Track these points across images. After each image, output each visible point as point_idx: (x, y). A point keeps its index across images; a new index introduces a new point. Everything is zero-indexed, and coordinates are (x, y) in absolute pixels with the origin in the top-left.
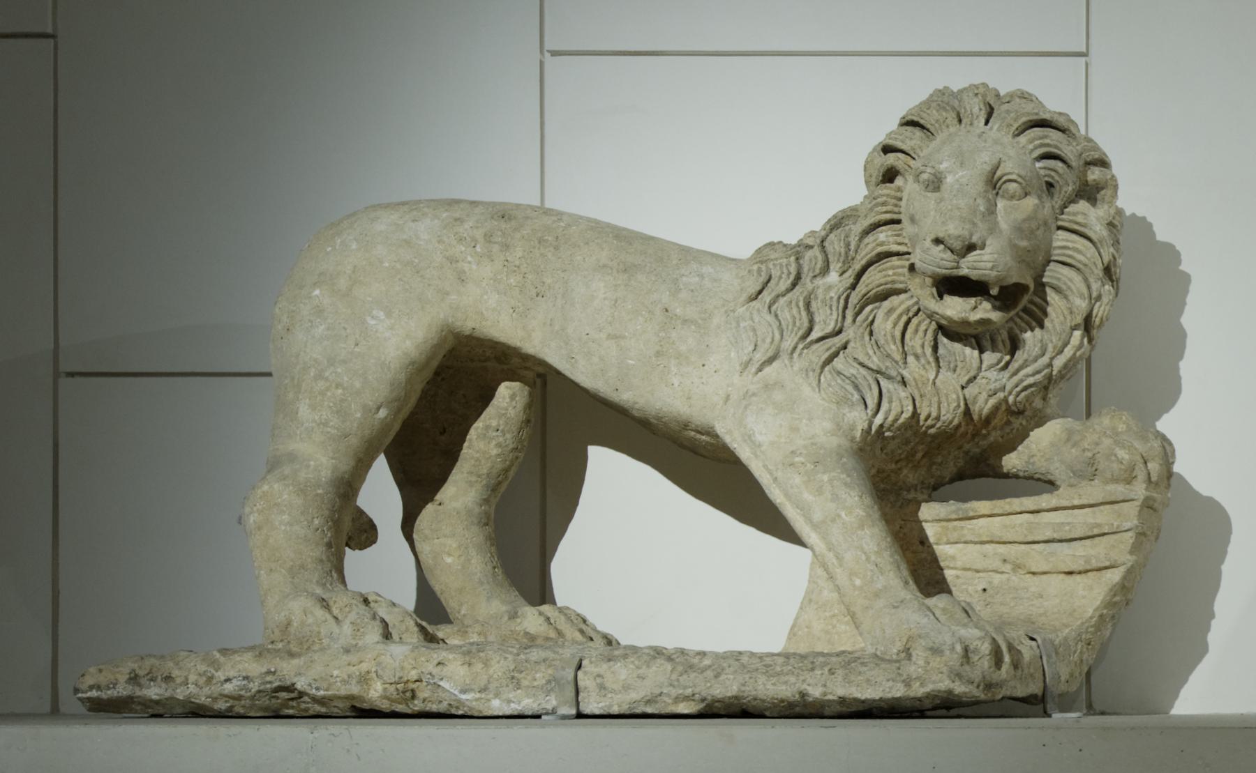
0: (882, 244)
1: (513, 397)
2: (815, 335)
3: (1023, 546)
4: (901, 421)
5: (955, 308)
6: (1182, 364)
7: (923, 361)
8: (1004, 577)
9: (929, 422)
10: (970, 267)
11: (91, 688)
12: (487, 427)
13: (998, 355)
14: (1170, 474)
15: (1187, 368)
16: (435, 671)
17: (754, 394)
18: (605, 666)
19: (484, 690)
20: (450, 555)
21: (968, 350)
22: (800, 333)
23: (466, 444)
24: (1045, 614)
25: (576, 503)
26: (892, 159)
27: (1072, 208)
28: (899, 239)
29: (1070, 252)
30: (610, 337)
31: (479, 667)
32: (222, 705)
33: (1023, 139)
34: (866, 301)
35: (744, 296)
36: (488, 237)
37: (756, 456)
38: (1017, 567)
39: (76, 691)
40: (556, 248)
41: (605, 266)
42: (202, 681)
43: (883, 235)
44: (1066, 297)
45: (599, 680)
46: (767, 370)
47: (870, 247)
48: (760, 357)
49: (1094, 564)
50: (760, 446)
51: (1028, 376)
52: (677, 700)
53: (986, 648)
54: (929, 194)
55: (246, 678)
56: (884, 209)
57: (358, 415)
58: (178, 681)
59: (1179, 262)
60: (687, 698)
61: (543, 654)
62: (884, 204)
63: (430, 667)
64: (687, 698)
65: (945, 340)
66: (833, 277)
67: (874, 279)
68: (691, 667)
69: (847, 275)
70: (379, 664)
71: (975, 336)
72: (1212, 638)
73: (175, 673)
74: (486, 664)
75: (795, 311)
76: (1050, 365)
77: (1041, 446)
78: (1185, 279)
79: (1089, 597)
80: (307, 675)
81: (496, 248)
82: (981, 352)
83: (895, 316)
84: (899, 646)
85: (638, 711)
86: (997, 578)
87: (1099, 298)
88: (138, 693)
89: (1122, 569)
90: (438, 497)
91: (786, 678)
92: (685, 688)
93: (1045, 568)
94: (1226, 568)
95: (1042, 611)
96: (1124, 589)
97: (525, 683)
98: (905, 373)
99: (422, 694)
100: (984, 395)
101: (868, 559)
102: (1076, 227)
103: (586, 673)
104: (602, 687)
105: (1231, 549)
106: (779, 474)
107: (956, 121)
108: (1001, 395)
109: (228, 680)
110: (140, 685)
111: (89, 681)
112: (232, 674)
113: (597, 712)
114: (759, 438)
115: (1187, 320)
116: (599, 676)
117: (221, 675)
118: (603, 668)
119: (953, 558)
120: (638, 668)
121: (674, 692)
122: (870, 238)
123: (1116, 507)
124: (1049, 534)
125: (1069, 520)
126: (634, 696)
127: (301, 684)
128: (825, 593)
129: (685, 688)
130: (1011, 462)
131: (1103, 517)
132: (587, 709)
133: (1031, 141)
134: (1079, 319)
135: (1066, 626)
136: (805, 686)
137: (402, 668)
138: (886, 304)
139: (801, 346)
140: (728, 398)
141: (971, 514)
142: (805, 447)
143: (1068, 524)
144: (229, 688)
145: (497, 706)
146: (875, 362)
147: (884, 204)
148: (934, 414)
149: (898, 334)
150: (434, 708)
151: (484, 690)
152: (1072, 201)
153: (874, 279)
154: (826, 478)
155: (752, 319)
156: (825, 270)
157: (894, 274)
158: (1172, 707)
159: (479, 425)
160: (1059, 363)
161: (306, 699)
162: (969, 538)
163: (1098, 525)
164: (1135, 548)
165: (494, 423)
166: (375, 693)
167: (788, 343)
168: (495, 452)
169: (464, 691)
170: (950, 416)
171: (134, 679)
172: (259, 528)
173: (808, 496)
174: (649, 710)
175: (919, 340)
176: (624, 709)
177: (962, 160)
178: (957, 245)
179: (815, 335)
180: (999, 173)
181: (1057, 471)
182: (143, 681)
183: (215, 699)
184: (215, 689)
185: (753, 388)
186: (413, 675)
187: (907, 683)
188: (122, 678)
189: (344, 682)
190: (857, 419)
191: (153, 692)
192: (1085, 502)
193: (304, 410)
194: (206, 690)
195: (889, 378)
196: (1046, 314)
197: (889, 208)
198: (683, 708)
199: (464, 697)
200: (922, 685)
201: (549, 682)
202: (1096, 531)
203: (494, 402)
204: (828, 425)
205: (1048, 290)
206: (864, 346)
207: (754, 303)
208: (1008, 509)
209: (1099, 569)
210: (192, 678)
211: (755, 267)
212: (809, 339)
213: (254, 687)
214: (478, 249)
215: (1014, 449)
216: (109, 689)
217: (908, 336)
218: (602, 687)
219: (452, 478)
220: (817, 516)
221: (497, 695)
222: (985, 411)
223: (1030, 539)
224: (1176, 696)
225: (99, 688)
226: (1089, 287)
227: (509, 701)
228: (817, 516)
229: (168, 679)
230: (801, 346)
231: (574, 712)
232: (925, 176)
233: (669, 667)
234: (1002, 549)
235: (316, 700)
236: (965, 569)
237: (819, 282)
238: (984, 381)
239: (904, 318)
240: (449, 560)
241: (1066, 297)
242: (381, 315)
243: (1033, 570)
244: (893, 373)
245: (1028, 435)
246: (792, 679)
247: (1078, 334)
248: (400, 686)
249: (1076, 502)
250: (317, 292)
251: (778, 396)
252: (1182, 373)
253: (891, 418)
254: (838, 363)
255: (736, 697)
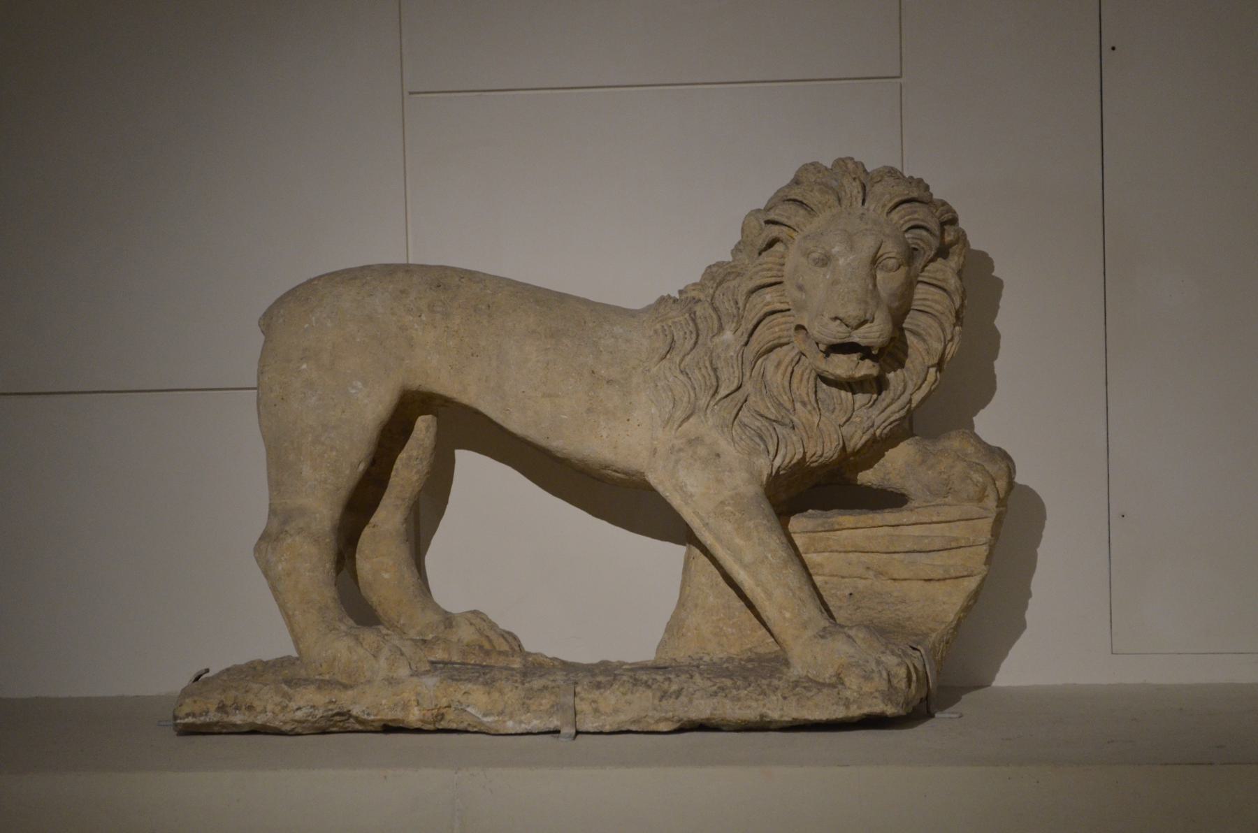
0: (768, 304)
1: (427, 428)
2: (723, 392)
3: (885, 556)
4: (795, 461)
5: (842, 366)
6: (996, 363)
7: (809, 407)
8: (869, 582)
9: (814, 458)
10: (857, 337)
11: (188, 715)
12: (410, 458)
13: (867, 396)
14: (1011, 484)
15: (1001, 366)
16: (463, 699)
17: (680, 450)
18: (597, 693)
19: (501, 713)
20: (387, 571)
21: (843, 393)
22: (711, 392)
23: (393, 473)
24: (909, 619)
25: (446, 503)
26: (775, 231)
27: (931, 266)
28: (783, 299)
29: (928, 303)
30: (544, 395)
31: (496, 695)
32: (288, 728)
33: (895, 216)
34: (760, 355)
35: (657, 358)
36: (431, 307)
37: (687, 504)
38: (879, 574)
39: (175, 718)
40: (490, 316)
41: (534, 332)
42: (277, 709)
43: (769, 296)
44: (924, 341)
45: (594, 705)
46: (686, 425)
47: (759, 306)
48: (679, 414)
49: (953, 573)
50: (691, 496)
51: (894, 413)
52: (658, 721)
53: (902, 672)
54: (818, 269)
55: (313, 707)
56: (770, 274)
57: (347, 472)
58: (259, 709)
59: (992, 268)
60: (667, 719)
61: (543, 682)
62: (769, 270)
63: (459, 696)
64: (667, 719)
65: (824, 386)
66: (728, 335)
67: (764, 336)
68: (665, 692)
69: (739, 333)
70: (418, 694)
71: (852, 385)
72: (1029, 616)
73: (256, 703)
74: (501, 692)
75: (704, 371)
76: (910, 401)
77: (895, 467)
78: (998, 284)
79: (948, 602)
80: (361, 704)
81: (438, 316)
82: (854, 393)
83: (782, 368)
84: (831, 671)
85: (624, 729)
86: (861, 584)
87: (952, 340)
88: (226, 719)
89: (978, 579)
90: (372, 520)
91: (749, 703)
92: (666, 712)
93: (907, 576)
94: (1041, 551)
95: (907, 615)
96: (976, 595)
97: (533, 707)
98: (795, 419)
99: (448, 717)
100: (860, 432)
101: (794, 594)
102: (934, 282)
103: (582, 699)
104: (596, 710)
105: (1046, 533)
106: (711, 521)
107: (836, 203)
108: (872, 430)
109: (299, 709)
110: (227, 713)
111: (186, 709)
112: (302, 704)
113: (592, 730)
114: (691, 489)
115: (1000, 323)
116: (594, 701)
117: (293, 705)
118: (596, 694)
119: (821, 565)
120: (624, 694)
121: (657, 715)
122: (755, 298)
123: (970, 523)
124: (909, 546)
125: (927, 533)
126: (622, 717)
127: (356, 711)
128: (711, 599)
129: (666, 712)
130: (867, 477)
131: (958, 531)
132: (581, 729)
133: (902, 218)
134: (936, 361)
135: (933, 630)
136: (765, 710)
137: (437, 697)
138: (773, 355)
139: (712, 403)
140: (655, 452)
141: (837, 527)
142: (732, 498)
143: (927, 537)
144: (299, 715)
145: (510, 726)
146: (772, 413)
147: (769, 270)
148: (819, 453)
149: (787, 384)
150: (454, 726)
151: (501, 713)
152: (932, 260)
153: (764, 336)
154: (751, 524)
155: (666, 378)
156: (721, 329)
157: (781, 330)
158: (993, 679)
159: (403, 455)
160: (917, 397)
161: (352, 720)
162: (837, 548)
163: (956, 539)
164: (989, 560)
165: (415, 453)
166: (414, 716)
167: (702, 402)
168: (415, 478)
169: (485, 715)
170: (831, 453)
171: (222, 708)
172: (289, 575)
173: (739, 541)
174: (634, 728)
175: (803, 388)
176: (615, 728)
177: (850, 241)
178: (854, 323)
179: (723, 392)
180: (881, 252)
181: (910, 486)
182: (229, 710)
183: (285, 723)
184: (289, 716)
185: (678, 443)
186: (444, 702)
187: (847, 706)
188: (213, 708)
189: (392, 709)
190: (765, 467)
191: (238, 718)
192: (943, 519)
193: (307, 470)
194: (281, 717)
195: (783, 425)
196: (906, 355)
197: (775, 273)
198: (663, 727)
199: (485, 719)
200: (859, 708)
201: (552, 706)
202: (954, 545)
203: (414, 434)
204: (745, 475)
205: (907, 334)
206: (763, 399)
207: (664, 362)
208: (870, 522)
209: (957, 578)
210: (269, 707)
211: (658, 326)
212: (718, 397)
213: (319, 713)
214: (423, 318)
215: (871, 466)
216: (201, 715)
217: (794, 386)
218: (596, 710)
219: (382, 503)
220: (748, 558)
221: (511, 718)
222: (859, 446)
223: (892, 549)
224: (996, 669)
225: (194, 715)
226: (943, 330)
227: (521, 722)
228: (748, 558)
229: (250, 708)
230: (712, 403)
231: (573, 731)
232: (816, 255)
233: (649, 693)
234: (865, 558)
235: (357, 719)
236: (832, 576)
237: (717, 340)
238: (858, 420)
239: (790, 369)
240: (386, 576)
241: (924, 341)
242: (359, 384)
243: (896, 576)
244: (787, 421)
245: (883, 456)
246: (754, 704)
247: (932, 370)
248: (435, 712)
249: (935, 519)
250: (304, 366)
251: (702, 451)
252: (997, 371)
253: (787, 460)
254: (745, 416)
255: (708, 719)
